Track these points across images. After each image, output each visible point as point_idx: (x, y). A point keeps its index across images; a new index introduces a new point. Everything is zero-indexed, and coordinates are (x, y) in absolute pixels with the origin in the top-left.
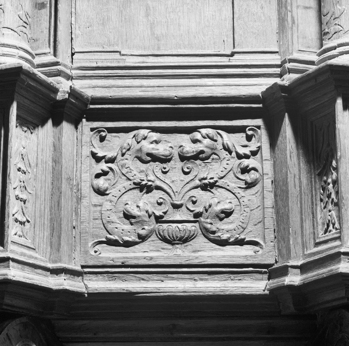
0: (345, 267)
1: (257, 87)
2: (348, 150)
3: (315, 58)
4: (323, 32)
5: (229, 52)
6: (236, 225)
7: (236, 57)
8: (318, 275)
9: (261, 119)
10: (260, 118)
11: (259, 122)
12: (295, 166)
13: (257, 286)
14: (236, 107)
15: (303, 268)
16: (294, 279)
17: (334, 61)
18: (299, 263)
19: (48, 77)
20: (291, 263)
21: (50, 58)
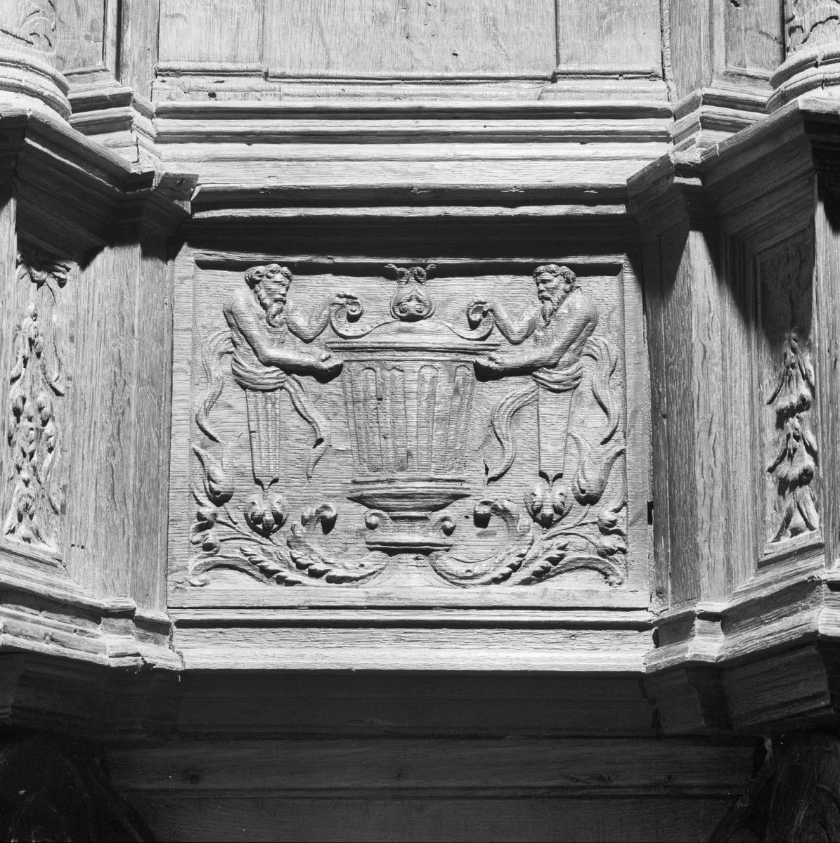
0: (823, 618)
1: (614, 165)
2: (4, 351)
3: (764, 94)
4: (787, 27)
5: (548, 73)
6: (527, 516)
7: (563, 84)
8: (552, 659)
9: (185, 247)
10: (179, 249)
11: (621, 259)
12: (613, 376)
13: (633, 655)
14: (438, 218)
15: (728, 620)
16: (708, 646)
17: (801, 102)
18: (719, 606)
19: (86, 134)
20: (700, 607)
21: (107, 86)
